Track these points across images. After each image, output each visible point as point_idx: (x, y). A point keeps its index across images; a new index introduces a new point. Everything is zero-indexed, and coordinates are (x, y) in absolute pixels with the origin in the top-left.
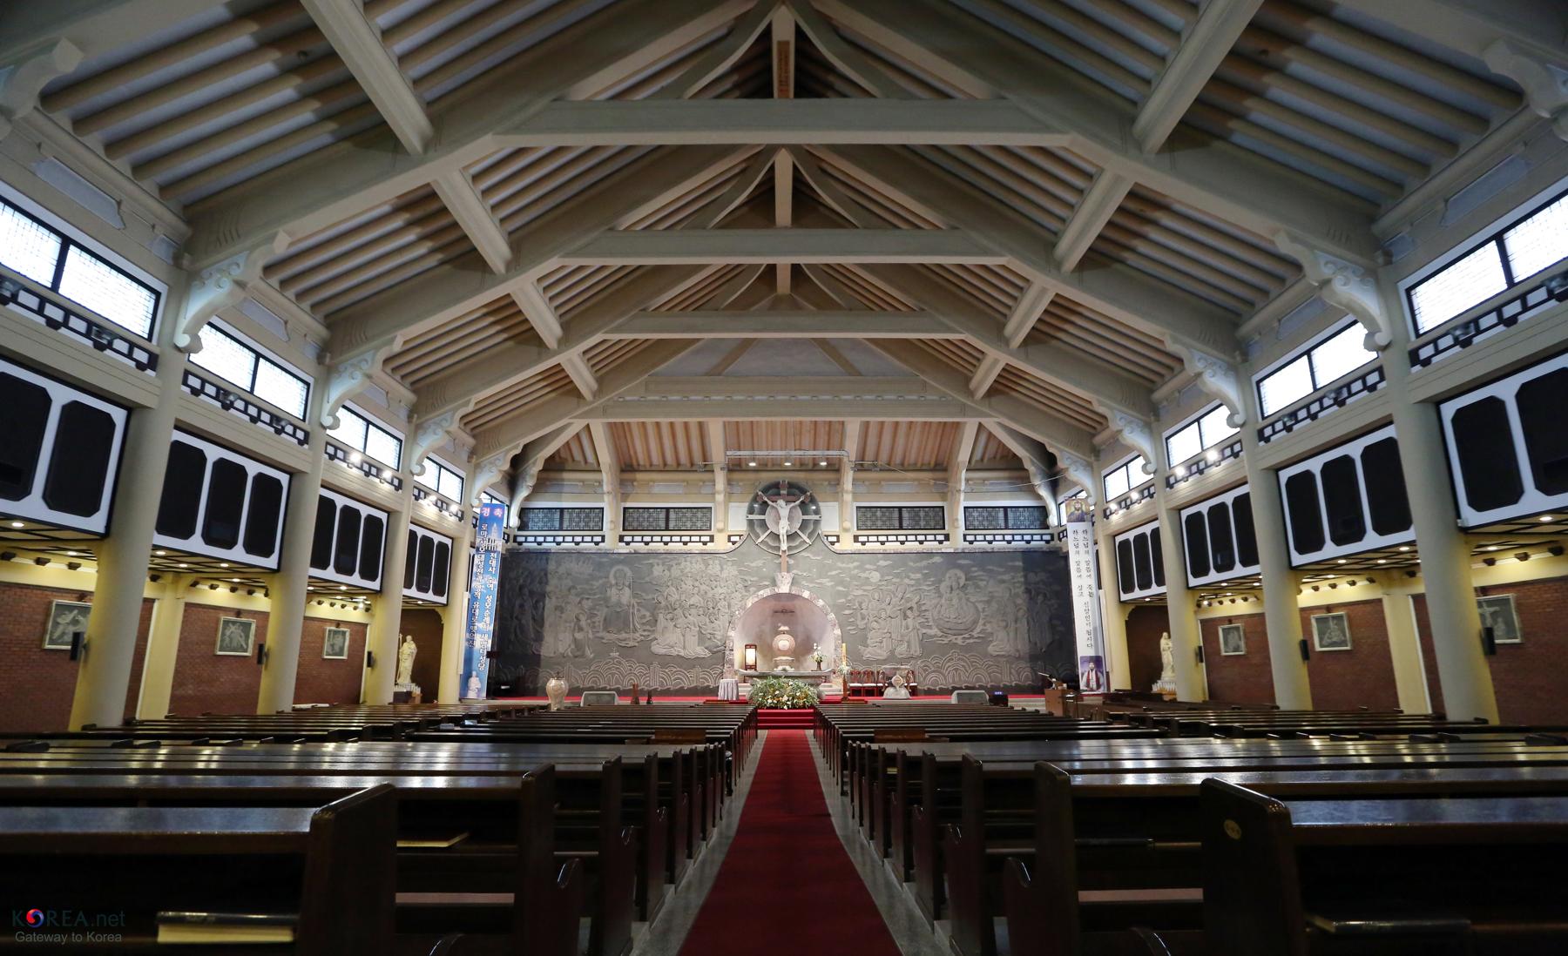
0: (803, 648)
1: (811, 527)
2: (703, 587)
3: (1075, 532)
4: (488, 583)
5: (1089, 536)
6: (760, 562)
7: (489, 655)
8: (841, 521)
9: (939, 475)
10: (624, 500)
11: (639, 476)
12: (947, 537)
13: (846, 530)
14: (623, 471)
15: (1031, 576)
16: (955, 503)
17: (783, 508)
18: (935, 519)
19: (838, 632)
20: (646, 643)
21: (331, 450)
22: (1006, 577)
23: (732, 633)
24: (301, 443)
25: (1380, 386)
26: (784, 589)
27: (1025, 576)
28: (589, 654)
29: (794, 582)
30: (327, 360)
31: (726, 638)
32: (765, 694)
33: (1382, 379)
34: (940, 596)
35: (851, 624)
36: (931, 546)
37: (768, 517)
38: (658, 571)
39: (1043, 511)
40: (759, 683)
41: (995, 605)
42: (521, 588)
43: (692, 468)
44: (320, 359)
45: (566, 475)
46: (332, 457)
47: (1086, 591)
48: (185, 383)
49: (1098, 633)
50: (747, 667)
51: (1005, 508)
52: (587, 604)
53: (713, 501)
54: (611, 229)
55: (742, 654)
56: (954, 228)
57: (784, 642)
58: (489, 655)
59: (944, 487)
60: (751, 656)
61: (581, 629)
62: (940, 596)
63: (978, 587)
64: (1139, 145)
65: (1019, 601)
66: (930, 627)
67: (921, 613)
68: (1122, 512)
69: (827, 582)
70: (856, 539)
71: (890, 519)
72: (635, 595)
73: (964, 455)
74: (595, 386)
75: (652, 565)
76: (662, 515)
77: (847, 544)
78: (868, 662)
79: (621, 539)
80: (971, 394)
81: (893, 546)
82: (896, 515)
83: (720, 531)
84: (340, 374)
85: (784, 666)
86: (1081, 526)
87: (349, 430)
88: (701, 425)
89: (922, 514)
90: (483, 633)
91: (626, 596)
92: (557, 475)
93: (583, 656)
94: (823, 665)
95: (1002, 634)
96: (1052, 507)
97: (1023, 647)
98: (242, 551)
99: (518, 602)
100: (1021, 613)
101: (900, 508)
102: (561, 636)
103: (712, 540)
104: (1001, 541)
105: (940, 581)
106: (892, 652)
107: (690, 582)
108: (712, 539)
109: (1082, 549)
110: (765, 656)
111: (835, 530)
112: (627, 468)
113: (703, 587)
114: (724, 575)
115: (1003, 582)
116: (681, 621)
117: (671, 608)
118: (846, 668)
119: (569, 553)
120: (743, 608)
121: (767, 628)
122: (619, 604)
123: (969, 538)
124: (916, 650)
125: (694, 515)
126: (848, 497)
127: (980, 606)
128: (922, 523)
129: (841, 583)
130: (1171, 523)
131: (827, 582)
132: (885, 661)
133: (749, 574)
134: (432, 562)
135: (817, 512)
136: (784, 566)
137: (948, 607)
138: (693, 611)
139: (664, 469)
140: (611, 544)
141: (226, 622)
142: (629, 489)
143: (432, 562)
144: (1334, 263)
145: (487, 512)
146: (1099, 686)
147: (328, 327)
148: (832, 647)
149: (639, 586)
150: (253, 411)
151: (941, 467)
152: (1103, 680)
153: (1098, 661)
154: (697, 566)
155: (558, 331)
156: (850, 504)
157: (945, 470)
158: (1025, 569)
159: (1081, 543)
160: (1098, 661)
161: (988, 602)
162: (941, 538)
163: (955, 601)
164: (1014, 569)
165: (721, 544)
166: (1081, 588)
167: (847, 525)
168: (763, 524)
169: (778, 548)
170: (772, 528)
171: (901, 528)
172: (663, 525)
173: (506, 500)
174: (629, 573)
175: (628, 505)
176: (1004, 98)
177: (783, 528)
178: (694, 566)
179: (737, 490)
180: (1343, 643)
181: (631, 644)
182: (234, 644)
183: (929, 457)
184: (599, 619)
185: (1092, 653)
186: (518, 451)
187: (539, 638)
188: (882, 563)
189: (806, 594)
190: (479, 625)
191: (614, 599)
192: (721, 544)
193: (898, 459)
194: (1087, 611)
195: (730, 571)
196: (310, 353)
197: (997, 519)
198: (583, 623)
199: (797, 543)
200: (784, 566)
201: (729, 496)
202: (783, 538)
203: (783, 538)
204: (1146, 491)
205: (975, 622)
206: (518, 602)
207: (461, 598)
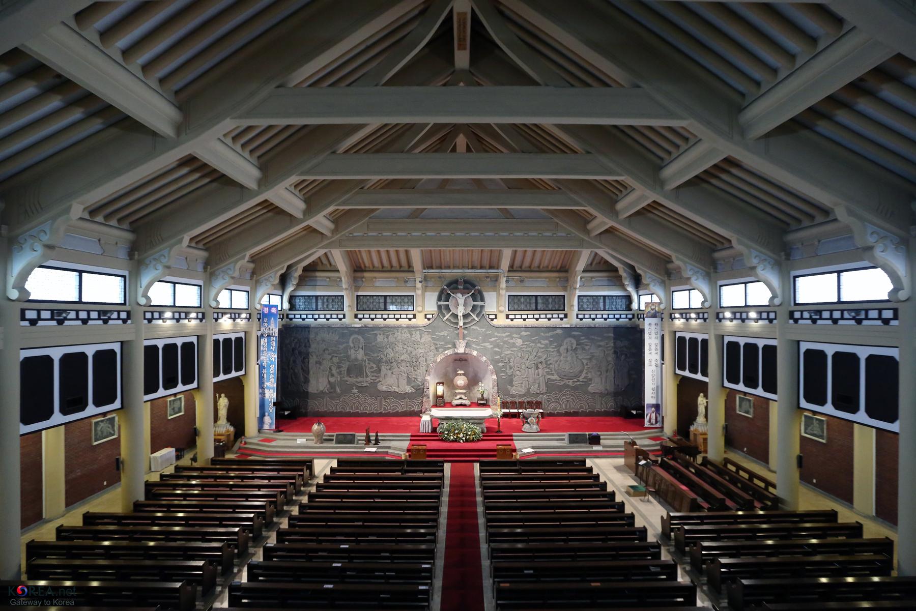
1: (479, 309)
2: (410, 349)
3: (650, 324)
4: (270, 357)
5: (659, 328)
7: (275, 404)
8: (498, 306)
9: (562, 275)
10: (357, 288)
11: (366, 275)
14: (355, 271)
15: (619, 343)
16: (571, 296)
17: (461, 298)
19: (495, 377)
20: (374, 384)
21: (148, 315)
22: (601, 343)
23: (428, 378)
24: (125, 321)
25: (893, 323)
26: (461, 350)
27: (615, 343)
28: (338, 390)
29: (467, 345)
30: (136, 257)
31: (424, 381)
33: (896, 317)
34: (560, 355)
36: (555, 322)
37: (450, 303)
38: (380, 338)
39: (629, 299)
41: (594, 361)
42: (293, 350)
44: (131, 255)
45: (318, 274)
46: (150, 321)
47: (654, 363)
48: (23, 318)
49: (659, 390)
51: (604, 297)
52: (336, 360)
54: (334, 152)
56: (588, 152)
57: (461, 381)
58: (275, 404)
61: (333, 375)
62: (560, 355)
63: (584, 349)
64: (742, 131)
65: (610, 359)
66: (553, 375)
67: (548, 365)
68: (683, 321)
71: (530, 303)
72: (366, 354)
75: (376, 335)
76: (382, 301)
77: (501, 321)
78: (513, 396)
80: (587, 232)
81: (531, 322)
82: (534, 300)
83: (419, 312)
84: (147, 266)
87: (160, 294)
88: (406, 251)
89: (550, 300)
90: (270, 388)
91: (360, 355)
92: (313, 274)
93: (335, 392)
95: (597, 380)
96: (635, 297)
97: (611, 389)
98: (93, 407)
99: (292, 359)
100: (611, 366)
101: (536, 296)
102: (320, 380)
105: (561, 345)
106: (529, 390)
107: (401, 346)
108: (414, 316)
109: (653, 335)
112: (358, 269)
113: (410, 349)
114: (423, 341)
115: (600, 346)
116: (396, 370)
117: (389, 362)
119: (322, 327)
120: (435, 362)
121: (450, 369)
122: (356, 359)
123: (580, 316)
124: (543, 389)
125: (402, 301)
126: (503, 284)
127: (585, 362)
128: (550, 306)
129: (498, 346)
130: (718, 349)
132: (523, 396)
133: (438, 340)
134: (232, 353)
135: (482, 299)
136: (461, 335)
137: (565, 362)
138: (403, 364)
139: (383, 270)
140: (349, 320)
141: (97, 424)
142: (360, 283)
143: (232, 353)
144: (878, 234)
145: (266, 310)
147: (133, 231)
149: (369, 348)
150: (83, 315)
151: (563, 270)
152: (659, 419)
153: (657, 407)
156: (505, 294)
158: (614, 339)
159: (653, 332)
160: (657, 407)
161: (590, 359)
162: (562, 316)
163: (569, 359)
164: (608, 338)
166: (650, 361)
167: (502, 308)
168: (447, 308)
170: (453, 311)
171: (536, 310)
173: (280, 293)
175: (360, 293)
176: (639, 87)
177: (460, 311)
178: (403, 335)
180: (821, 437)
181: (365, 384)
182: (105, 434)
183: (557, 262)
184: (344, 369)
185: (654, 402)
186: (283, 271)
187: (307, 381)
188: (524, 333)
189: (475, 353)
190: (267, 384)
191: (353, 357)
192: (420, 321)
193: (536, 263)
194: (653, 375)
196: (122, 254)
197: (598, 303)
198: (334, 372)
200: (461, 335)
201: (425, 289)
204: (701, 313)
205: (581, 372)
206: (292, 359)
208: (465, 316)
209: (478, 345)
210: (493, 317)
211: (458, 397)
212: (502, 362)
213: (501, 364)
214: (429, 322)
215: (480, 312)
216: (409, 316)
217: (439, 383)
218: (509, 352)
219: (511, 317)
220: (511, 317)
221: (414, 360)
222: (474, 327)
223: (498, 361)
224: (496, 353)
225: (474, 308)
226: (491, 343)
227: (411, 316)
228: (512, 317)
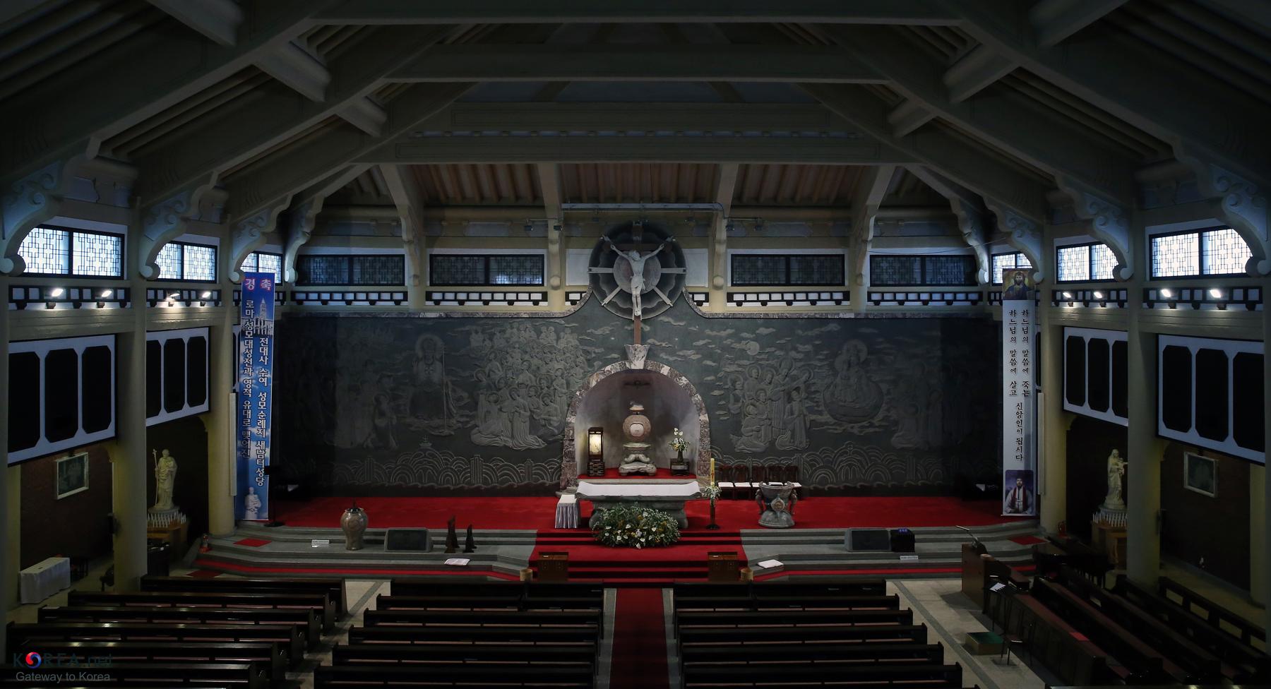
1: (673, 283)
2: (535, 362)
4: (259, 377)
5: (1030, 319)
8: (712, 276)
10: (432, 241)
11: (449, 213)
12: (847, 296)
13: (718, 288)
18: (829, 273)
19: (704, 417)
23: (572, 419)
26: (638, 364)
28: (393, 443)
29: (651, 355)
31: (564, 426)
32: (614, 526)
33: (707, 300)
35: (721, 408)
36: (825, 306)
37: (617, 271)
38: (476, 340)
43: (517, 204)
49: (1031, 443)
51: (923, 257)
57: (637, 426)
59: (848, 231)
60: (596, 441)
61: (382, 414)
66: (820, 413)
69: (692, 355)
70: (730, 298)
73: (876, 197)
74: (380, 117)
75: (469, 333)
77: (718, 306)
78: (742, 455)
79: (429, 296)
82: (782, 266)
83: (555, 288)
86: (1020, 305)
89: (816, 265)
90: (258, 439)
103: (545, 298)
104: (914, 301)
106: (772, 443)
107: (517, 355)
109: (1020, 335)
111: (704, 284)
114: (562, 344)
117: (494, 387)
123: (875, 297)
124: (801, 439)
127: (884, 387)
128: (816, 277)
129: (710, 356)
131: (692, 355)
135: (681, 262)
136: (637, 334)
146: (1026, 507)
154: (527, 335)
155: (322, 76)
156: (725, 252)
157: (848, 207)
159: (1019, 328)
160: (1027, 477)
162: (838, 296)
167: (719, 281)
168: (611, 281)
169: (630, 311)
172: (482, 279)
174: (440, 343)
175: (437, 251)
181: (446, 432)
185: (1020, 466)
188: (763, 331)
189: (665, 370)
192: (557, 305)
197: (911, 271)
200: (637, 334)
201: (566, 242)
205: (877, 407)
207: (228, 402)
208: (647, 296)
209: (673, 353)
211: (632, 457)
212: (719, 387)
213: (716, 393)
217: (593, 431)
220: (737, 297)
224: (708, 370)
225: (664, 282)
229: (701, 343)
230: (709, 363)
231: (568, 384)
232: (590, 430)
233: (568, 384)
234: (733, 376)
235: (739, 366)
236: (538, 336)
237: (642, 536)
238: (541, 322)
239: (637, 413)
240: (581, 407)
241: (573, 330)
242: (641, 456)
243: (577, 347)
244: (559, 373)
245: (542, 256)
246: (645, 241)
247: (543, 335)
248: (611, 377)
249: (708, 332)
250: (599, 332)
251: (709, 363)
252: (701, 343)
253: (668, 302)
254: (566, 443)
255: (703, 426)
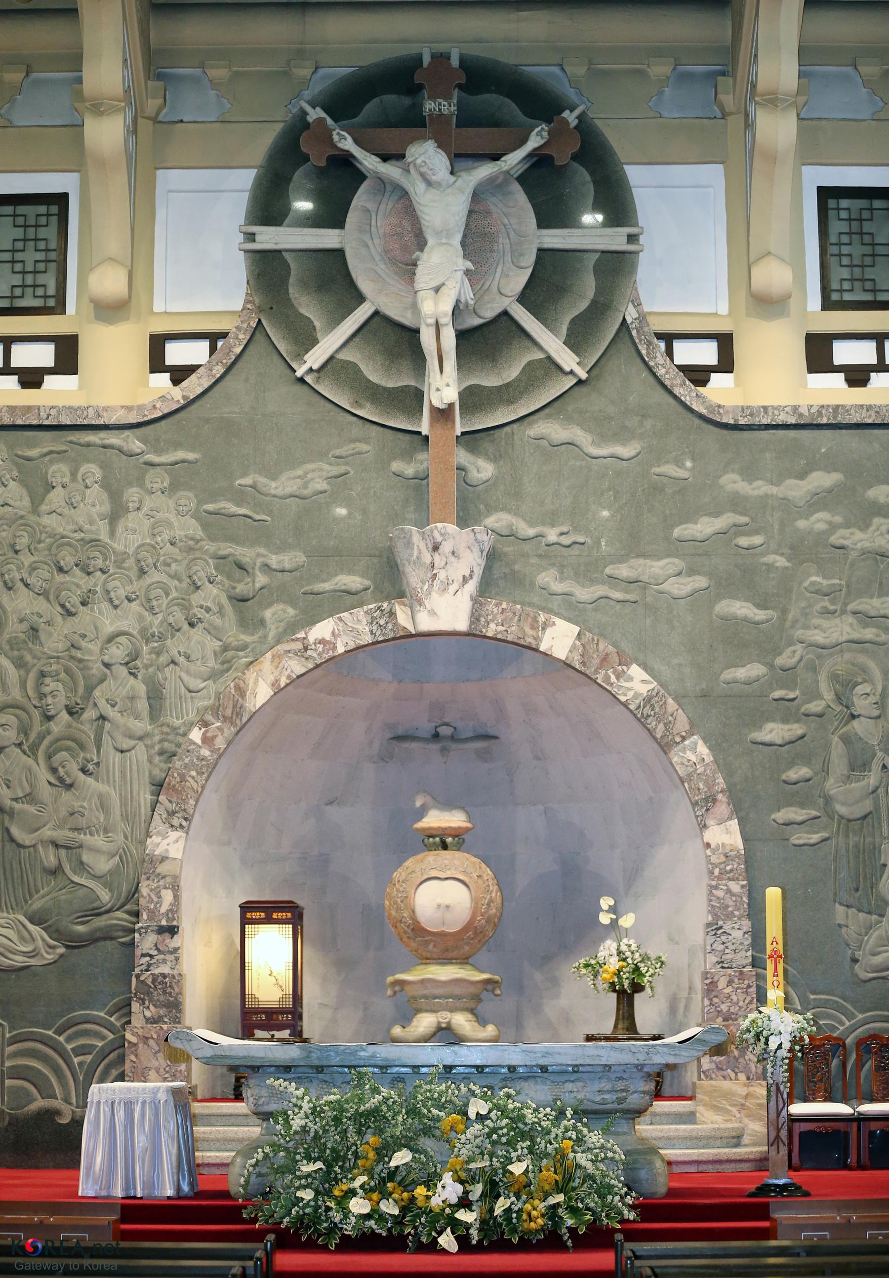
0: (539, 925)
6: (313, 473)
8: (743, 253)
13: (768, 305)
17: (438, 187)
19: (726, 834)
23: (168, 844)
26: (446, 608)
29: (497, 575)
31: (138, 867)
32: (337, 1163)
33: (726, 364)
35: (796, 793)
37: (360, 239)
40: (301, 1102)
50: (252, 1019)
53: (75, 155)
55: (223, 951)
70: (818, 353)
77: (771, 379)
83: (110, 311)
85: (442, 1040)
94: (648, 1012)
108: (68, 356)
110: (343, 965)
114: (131, 535)
118: (783, 1024)
120: (230, 710)
121: (356, 819)
126: (777, 129)
129: (743, 578)
131: (670, 578)
133: (261, 535)
135: (618, 206)
136: (443, 490)
148: (696, 916)
165: (114, 380)
167: (773, 275)
168: (334, 278)
169: (411, 399)
170: (379, 294)
177: (438, 293)
179: (197, 105)
189: (559, 639)
192: (114, 380)
195: (161, 518)
199: (512, 371)
200: (443, 490)
201: (157, 140)
202: (440, 342)
203: (440, 342)
208: (481, 340)
209: (588, 572)
210: (705, 354)
211: (425, 1022)
212: (787, 711)
213: (774, 732)
214: (178, 394)
215: (599, 309)
216: (26, 356)
217: (256, 912)
218: (841, 629)
219: (846, 353)
220: (846, 353)
221: (58, 695)
222: (552, 429)
223: (750, 706)
224: (738, 640)
225: (547, 282)
226: (695, 555)
227: (42, 355)
228: (860, 353)
229: (705, 527)
230: (741, 608)
231: (155, 696)
232: (246, 908)
233: (155, 696)
234: (839, 663)
235: (865, 618)
236: (36, 501)
237: (464, 1203)
238: (47, 442)
239: (442, 841)
240: (209, 807)
241: (180, 478)
242: (462, 1021)
243: (191, 548)
244: (117, 652)
245: (61, 200)
246: (467, 119)
247: (56, 497)
248: (337, 668)
249: (733, 482)
250: (284, 485)
251: (741, 608)
252: (705, 527)
253: (567, 359)
254: (147, 943)
255: (717, 874)
